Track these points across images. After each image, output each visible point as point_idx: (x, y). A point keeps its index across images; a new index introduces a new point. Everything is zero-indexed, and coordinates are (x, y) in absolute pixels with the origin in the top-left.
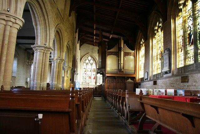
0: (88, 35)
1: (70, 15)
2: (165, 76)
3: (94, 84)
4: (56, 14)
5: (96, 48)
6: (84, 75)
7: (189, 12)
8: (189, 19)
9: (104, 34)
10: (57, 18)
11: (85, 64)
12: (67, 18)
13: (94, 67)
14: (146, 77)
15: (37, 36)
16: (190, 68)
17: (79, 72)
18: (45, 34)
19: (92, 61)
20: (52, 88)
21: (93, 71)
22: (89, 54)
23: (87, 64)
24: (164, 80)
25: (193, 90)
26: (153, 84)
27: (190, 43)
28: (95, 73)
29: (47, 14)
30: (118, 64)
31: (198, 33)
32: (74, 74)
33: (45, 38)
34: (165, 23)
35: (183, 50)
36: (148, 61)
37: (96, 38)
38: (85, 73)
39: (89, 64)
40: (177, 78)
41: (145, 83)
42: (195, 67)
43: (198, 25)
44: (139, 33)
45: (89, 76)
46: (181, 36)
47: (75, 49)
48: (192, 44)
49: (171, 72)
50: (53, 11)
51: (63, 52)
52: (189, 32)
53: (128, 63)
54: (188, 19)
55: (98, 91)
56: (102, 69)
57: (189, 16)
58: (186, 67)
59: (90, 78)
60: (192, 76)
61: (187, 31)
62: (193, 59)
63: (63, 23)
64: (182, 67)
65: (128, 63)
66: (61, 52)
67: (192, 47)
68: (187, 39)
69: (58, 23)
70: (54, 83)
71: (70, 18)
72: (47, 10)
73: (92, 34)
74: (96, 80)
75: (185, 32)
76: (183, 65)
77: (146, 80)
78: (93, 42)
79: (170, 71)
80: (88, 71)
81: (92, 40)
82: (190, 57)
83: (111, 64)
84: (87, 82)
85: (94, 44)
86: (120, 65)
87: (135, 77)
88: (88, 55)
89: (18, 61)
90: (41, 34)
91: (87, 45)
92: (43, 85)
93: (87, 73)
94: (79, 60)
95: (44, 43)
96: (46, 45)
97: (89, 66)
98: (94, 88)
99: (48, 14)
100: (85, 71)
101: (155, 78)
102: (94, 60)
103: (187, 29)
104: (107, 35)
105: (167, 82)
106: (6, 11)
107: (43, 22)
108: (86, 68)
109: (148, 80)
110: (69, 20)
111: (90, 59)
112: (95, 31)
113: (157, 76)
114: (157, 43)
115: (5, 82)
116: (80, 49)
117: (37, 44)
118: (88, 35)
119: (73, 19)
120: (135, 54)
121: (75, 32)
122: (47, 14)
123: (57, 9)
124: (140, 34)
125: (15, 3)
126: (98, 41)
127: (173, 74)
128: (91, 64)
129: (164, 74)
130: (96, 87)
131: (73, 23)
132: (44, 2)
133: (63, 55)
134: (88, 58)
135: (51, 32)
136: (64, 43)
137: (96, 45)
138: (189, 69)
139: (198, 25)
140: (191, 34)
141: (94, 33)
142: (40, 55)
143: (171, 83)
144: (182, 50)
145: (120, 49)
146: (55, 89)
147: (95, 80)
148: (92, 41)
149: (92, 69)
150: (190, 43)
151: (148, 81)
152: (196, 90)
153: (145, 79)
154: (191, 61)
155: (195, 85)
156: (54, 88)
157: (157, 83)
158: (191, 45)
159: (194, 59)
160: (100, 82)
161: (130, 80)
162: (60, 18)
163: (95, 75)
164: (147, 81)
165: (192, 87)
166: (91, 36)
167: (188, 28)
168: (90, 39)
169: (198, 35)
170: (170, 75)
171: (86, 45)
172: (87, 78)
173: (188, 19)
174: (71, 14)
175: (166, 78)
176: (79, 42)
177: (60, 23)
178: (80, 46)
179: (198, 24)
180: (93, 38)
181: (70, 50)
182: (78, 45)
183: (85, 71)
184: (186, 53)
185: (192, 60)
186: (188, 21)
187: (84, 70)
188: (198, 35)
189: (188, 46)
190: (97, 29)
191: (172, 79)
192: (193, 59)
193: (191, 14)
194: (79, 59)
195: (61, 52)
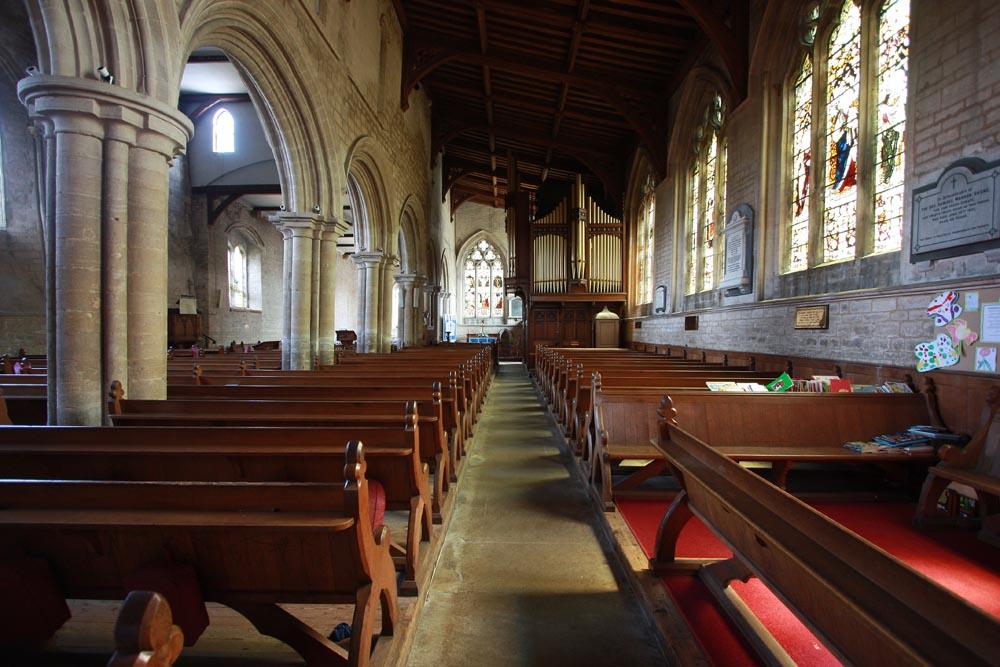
0: (476, 174)
1: (404, 105)
2: (728, 301)
3: (498, 322)
4: (344, 100)
5: (501, 214)
6: (470, 297)
7: (844, 55)
8: (842, 83)
9: (522, 166)
10: (352, 113)
11: (470, 265)
12: (395, 117)
13: (498, 272)
14: (659, 304)
15: (285, 181)
16: (833, 276)
17: (452, 289)
18: (312, 172)
19: (490, 256)
20: (363, 347)
23: (477, 263)
24: (724, 316)
25: (849, 359)
26: (683, 325)
27: (838, 180)
28: (501, 290)
29: (308, 97)
31: (880, 137)
32: (436, 295)
33: (314, 188)
34: (735, 112)
35: (806, 208)
36: (666, 248)
37: (498, 183)
38: (473, 290)
39: (484, 264)
40: (775, 310)
41: (655, 321)
42: (858, 272)
43: (885, 102)
44: (637, 156)
45: (484, 299)
46: (802, 156)
47: (432, 219)
48: (850, 182)
49: (756, 284)
50: (331, 87)
51: (390, 231)
52: (837, 136)
54: (837, 84)
55: (501, 347)
56: (520, 280)
57: (841, 72)
58: (816, 276)
60: (844, 308)
61: (829, 132)
62: (848, 239)
63: (379, 135)
64: (801, 273)
65: (601, 264)
66: (382, 232)
67: (852, 193)
68: (828, 163)
69: (359, 134)
70: (367, 331)
71: (407, 115)
72: (307, 83)
73: (486, 169)
74: (504, 310)
75: (818, 139)
77: (661, 312)
78: (492, 193)
79: (749, 286)
80: (480, 285)
81: (486, 188)
82: (838, 234)
83: (547, 269)
84: (479, 315)
85: (496, 202)
86: (573, 264)
87: (622, 303)
89: (262, 265)
90: (295, 173)
91: (475, 206)
92: (321, 346)
94: (453, 253)
95: (310, 203)
96: (318, 212)
97: (483, 270)
99: (313, 98)
100: (472, 286)
101: (691, 305)
102: (497, 250)
103: (829, 124)
104: (533, 169)
105: (739, 323)
106: (97, 79)
107: (297, 130)
109: (667, 312)
110: (402, 124)
111: (483, 250)
112: (493, 159)
113: (697, 300)
114: (708, 183)
115: (134, 363)
116: (452, 220)
117: (288, 209)
118: (476, 174)
119: (416, 117)
120: (622, 229)
121: (429, 164)
122: (308, 97)
123: (349, 82)
124: (640, 160)
125: (132, 44)
126: (504, 192)
127: (761, 298)
128: (490, 264)
129: (727, 296)
130: (505, 332)
131: (419, 135)
132: (289, 50)
133: (390, 243)
134: (480, 246)
135: (333, 164)
136: (392, 201)
137: (500, 206)
138: (831, 281)
139: (885, 102)
140: (849, 142)
141: (491, 167)
142: (301, 247)
143: (754, 330)
144: (801, 208)
145: (573, 216)
146: (374, 351)
147: (502, 311)
148: (487, 192)
150: (838, 180)
151: (668, 316)
152: (860, 360)
153: (658, 310)
154: (840, 252)
155: (857, 343)
156: (371, 347)
157: (700, 324)
158: (841, 190)
159: (852, 241)
160: (516, 316)
162: (366, 115)
163: (502, 296)
164: (663, 316)
165: (844, 348)
166: (483, 176)
167: (835, 120)
168: (481, 186)
169: (880, 145)
170: (750, 298)
171: (469, 207)
172: (480, 305)
173: (837, 84)
174: (410, 102)
175: (735, 308)
176: (448, 196)
177: (366, 133)
178: (454, 208)
179: (882, 98)
180: (492, 182)
183: (472, 286)
184: (819, 218)
185: (843, 245)
186: (836, 92)
187: (468, 282)
188: (880, 145)
189: (828, 191)
190: (500, 152)
191: (759, 312)
192: (848, 239)
193: (854, 62)
194: (453, 247)
195: (382, 232)
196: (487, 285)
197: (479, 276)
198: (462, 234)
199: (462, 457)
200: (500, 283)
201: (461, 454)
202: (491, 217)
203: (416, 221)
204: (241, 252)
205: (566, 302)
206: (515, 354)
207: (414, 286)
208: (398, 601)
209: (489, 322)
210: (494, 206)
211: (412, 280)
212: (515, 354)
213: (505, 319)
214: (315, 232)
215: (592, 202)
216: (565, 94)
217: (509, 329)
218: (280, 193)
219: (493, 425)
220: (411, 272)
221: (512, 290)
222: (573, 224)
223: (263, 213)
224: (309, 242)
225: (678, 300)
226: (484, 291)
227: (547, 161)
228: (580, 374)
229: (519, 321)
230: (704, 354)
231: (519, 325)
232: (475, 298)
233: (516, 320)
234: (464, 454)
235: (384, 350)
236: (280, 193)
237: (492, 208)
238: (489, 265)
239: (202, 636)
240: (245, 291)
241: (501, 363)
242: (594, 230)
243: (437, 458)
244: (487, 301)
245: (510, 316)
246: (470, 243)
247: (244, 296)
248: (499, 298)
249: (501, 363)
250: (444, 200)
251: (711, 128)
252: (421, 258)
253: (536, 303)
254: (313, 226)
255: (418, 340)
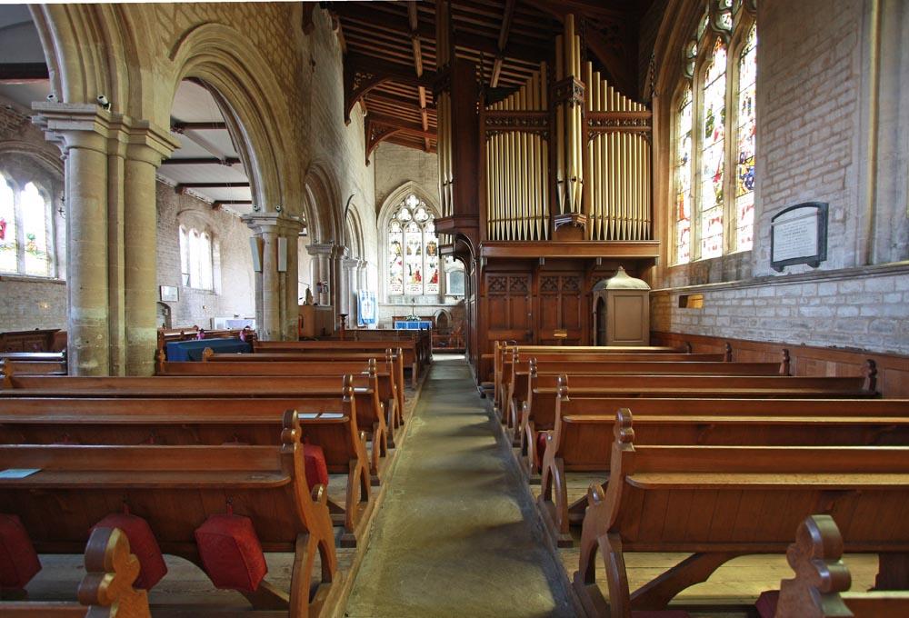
3: (434, 301)
6: (397, 269)
11: (396, 227)
17: (371, 254)
19: (421, 215)
21: (428, 252)
22: (409, 186)
23: (404, 224)
30: (553, 183)
38: (400, 259)
39: (413, 226)
45: (414, 272)
53: (607, 189)
56: (463, 227)
59: (418, 277)
74: (441, 285)
76: (718, 254)
78: (420, 127)
80: (409, 253)
83: (515, 201)
84: (409, 292)
86: (560, 188)
88: (404, 190)
91: (400, 149)
93: (408, 259)
95: (95, 85)
97: (413, 235)
98: (437, 315)
102: (429, 207)
108: (400, 240)
109: (839, 257)
111: (413, 207)
116: (367, 162)
130: (442, 314)
134: (408, 202)
141: (414, 69)
145: (560, 93)
147: (437, 286)
149: (426, 245)
160: (456, 293)
161: (620, 281)
163: (437, 267)
172: (409, 279)
178: (370, 146)
181: (272, 118)
182: (353, 135)
187: (394, 248)
196: (418, 254)
197: (407, 240)
198: (383, 188)
199: (400, 427)
200: (435, 250)
201: (399, 423)
202: (422, 164)
203: (268, 107)
204: (207, 237)
205: (547, 259)
206: (454, 344)
207: (277, 233)
208: (338, 553)
209: (421, 301)
210: (425, 149)
211: (274, 223)
212: (454, 344)
213: (441, 298)
214: (112, 141)
215: (594, 71)
216: (497, 75)
217: (447, 309)
218: (46, 76)
219: (423, 480)
220: (271, 208)
221: (450, 250)
222: (560, 108)
223: (190, 190)
224: (100, 160)
225: (881, 232)
226: (413, 259)
227: (501, 44)
228: (516, 359)
229: (460, 299)
230: (873, 364)
231: (461, 305)
232: (398, 270)
233: (456, 298)
234: (402, 423)
235: (131, 363)
236: (46, 76)
237: (422, 152)
238: (420, 227)
239: (164, 578)
240: (52, 253)
241: (436, 358)
242: (597, 124)
243: (374, 426)
244: (418, 273)
245: (448, 293)
246: (396, 196)
247: (49, 259)
248: (434, 270)
249: (436, 358)
250: (347, 119)
251: (714, 33)
252: (289, 186)
253: (491, 260)
254: (102, 129)
255: (291, 328)
